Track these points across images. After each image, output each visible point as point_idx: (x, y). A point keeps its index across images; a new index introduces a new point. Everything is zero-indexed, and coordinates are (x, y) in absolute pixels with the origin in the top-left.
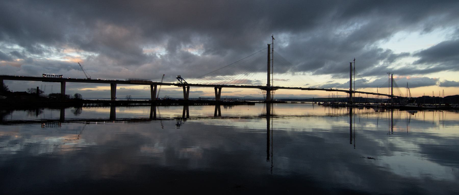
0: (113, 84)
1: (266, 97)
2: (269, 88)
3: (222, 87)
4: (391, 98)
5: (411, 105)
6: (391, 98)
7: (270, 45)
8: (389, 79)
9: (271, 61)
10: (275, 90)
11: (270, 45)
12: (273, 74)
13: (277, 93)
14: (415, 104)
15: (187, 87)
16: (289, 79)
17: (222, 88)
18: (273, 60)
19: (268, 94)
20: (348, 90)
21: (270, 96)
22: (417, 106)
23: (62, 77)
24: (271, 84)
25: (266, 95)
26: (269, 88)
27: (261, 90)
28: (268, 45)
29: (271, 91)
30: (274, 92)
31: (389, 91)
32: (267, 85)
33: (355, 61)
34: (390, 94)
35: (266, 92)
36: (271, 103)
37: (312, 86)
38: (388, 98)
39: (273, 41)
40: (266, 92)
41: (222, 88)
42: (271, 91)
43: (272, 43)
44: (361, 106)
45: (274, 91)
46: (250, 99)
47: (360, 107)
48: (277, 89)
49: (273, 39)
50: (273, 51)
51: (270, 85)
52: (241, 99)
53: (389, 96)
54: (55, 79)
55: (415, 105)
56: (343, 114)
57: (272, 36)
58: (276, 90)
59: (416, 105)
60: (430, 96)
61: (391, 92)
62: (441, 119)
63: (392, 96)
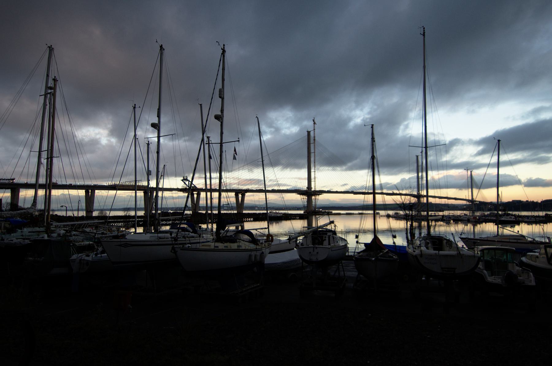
0: (90, 190)
1: (306, 206)
2: (309, 193)
3: (246, 193)
4: (471, 203)
5: (508, 218)
6: (471, 203)
7: (310, 131)
8: (468, 177)
9: (312, 155)
10: (319, 195)
11: (310, 131)
12: (365, 186)
13: (322, 199)
14: (512, 217)
15: (196, 193)
16: (347, 183)
17: (246, 194)
18: (314, 152)
19: (309, 201)
20: (415, 193)
21: (312, 204)
22: (514, 220)
23: (13, 182)
24: (313, 186)
25: (306, 203)
26: (309, 193)
27: (299, 195)
28: (307, 132)
29: (313, 197)
30: (317, 198)
31: (468, 194)
32: (307, 188)
33: (422, 153)
34: (470, 198)
35: (306, 198)
36: (313, 215)
37: (357, 185)
38: (464, 202)
39: (314, 127)
40: (306, 199)
41: (246, 194)
42: (313, 197)
43: (313, 129)
44: (448, 219)
45: (317, 197)
46: (274, 207)
47: (447, 220)
48: (321, 194)
49: (314, 123)
50: (314, 140)
51: (312, 188)
52: (262, 208)
53: (468, 200)
54: (17, 184)
55: (512, 218)
56: (450, 227)
57: (313, 120)
58: (320, 195)
59: (513, 218)
60: (522, 200)
61: (471, 195)
62: (467, 227)
63: (472, 201)
